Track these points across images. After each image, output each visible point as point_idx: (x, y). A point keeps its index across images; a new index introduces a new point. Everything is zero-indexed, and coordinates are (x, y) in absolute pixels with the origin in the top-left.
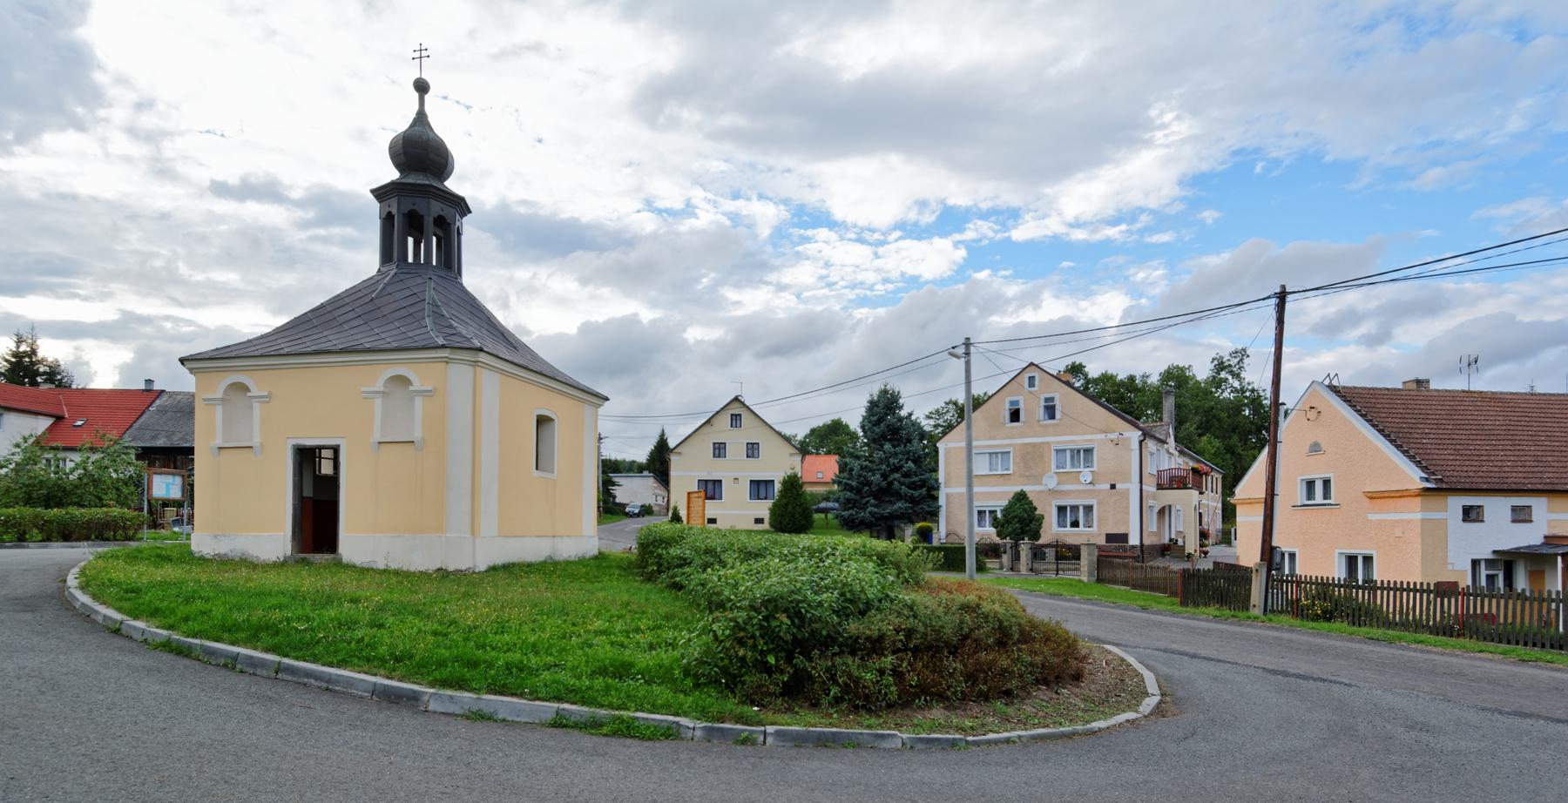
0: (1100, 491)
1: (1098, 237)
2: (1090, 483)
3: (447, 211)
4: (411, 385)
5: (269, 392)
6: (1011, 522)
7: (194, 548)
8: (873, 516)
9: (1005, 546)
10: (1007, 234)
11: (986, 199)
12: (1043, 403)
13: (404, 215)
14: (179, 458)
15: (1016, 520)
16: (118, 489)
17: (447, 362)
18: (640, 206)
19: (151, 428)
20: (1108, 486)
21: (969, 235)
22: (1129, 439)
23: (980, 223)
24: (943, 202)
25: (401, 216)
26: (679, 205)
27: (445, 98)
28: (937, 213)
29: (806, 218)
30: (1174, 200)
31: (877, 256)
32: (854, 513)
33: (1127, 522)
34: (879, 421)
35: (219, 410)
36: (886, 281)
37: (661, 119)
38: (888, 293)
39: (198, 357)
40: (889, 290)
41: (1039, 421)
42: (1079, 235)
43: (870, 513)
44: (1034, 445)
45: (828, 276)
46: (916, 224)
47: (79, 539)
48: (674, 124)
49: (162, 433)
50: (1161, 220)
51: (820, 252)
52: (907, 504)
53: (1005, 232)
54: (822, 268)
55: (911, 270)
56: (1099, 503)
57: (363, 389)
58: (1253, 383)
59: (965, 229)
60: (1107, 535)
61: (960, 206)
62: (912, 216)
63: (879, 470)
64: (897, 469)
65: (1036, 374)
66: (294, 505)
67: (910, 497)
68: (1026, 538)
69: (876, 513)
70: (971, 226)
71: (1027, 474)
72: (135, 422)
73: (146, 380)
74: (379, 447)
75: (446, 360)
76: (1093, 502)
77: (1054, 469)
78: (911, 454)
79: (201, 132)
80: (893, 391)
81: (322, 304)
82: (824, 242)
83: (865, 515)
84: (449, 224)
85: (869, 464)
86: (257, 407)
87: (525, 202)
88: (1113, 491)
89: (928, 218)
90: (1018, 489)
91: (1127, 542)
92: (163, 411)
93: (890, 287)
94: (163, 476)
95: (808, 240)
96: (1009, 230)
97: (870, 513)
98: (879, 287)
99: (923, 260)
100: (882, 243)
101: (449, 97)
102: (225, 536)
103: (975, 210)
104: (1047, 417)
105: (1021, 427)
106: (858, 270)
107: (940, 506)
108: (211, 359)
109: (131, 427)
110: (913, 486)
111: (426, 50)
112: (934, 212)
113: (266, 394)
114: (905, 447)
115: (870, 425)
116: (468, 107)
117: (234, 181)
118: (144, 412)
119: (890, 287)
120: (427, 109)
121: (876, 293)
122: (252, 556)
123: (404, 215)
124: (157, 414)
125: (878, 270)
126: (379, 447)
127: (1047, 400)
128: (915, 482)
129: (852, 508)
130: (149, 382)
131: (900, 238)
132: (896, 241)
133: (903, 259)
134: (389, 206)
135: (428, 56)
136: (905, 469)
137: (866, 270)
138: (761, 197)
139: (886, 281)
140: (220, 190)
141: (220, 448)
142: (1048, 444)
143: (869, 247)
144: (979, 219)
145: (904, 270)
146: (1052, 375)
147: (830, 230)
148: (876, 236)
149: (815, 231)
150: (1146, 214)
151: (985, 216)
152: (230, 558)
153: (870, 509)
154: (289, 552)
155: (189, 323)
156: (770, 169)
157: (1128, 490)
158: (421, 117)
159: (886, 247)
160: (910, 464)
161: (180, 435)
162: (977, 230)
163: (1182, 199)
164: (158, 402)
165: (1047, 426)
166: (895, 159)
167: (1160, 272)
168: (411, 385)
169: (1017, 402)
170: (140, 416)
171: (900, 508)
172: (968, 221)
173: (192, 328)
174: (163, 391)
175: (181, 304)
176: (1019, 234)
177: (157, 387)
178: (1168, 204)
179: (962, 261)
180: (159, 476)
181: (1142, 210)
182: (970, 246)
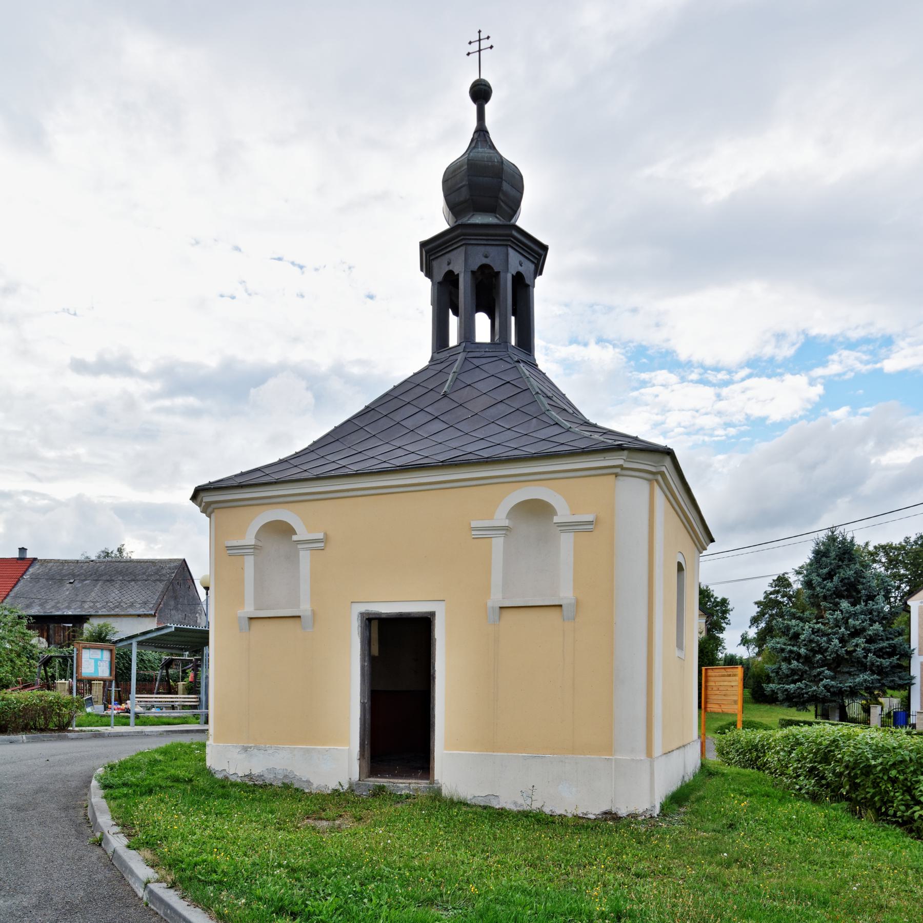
5: (326, 534)
7: (212, 761)
8: (828, 691)
10: (878, 366)
11: (857, 327)
13: (473, 272)
14: (51, 626)
16: (12, 661)
17: (617, 475)
19: (25, 596)
21: (834, 368)
23: (845, 353)
24: (804, 332)
25: (469, 274)
27: (280, 259)
28: (797, 346)
29: (644, 360)
31: (719, 397)
32: (802, 686)
34: (830, 576)
35: (249, 562)
36: (728, 425)
38: (729, 437)
40: (730, 435)
43: (825, 686)
45: (663, 423)
46: (772, 360)
47: (16, 731)
49: (36, 601)
51: (657, 396)
52: (875, 676)
53: (876, 363)
54: (657, 414)
55: (756, 411)
59: (827, 362)
61: (825, 336)
62: (769, 351)
63: (835, 634)
64: (856, 633)
67: (878, 666)
69: (832, 686)
70: (835, 357)
72: (11, 590)
73: (19, 549)
74: (500, 614)
75: (618, 470)
78: (875, 614)
79: (56, 313)
80: (845, 539)
81: (367, 407)
82: (662, 385)
83: (818, 689)
84: (528, 286)
85: (822, 627)
86: (305, 557)
87: (360, 362)
89: (787, 351)
92: (36, 579)
93: (732, 431)
94: (92, 651)
95: (644, 384)
97: (825, 686)
98: (720, 432)
99: (772, 399)
100: (726, 383)
103: (841, 339)
106: (697, 415)
107: (913, 678)
108: (241, 486)
109: (8, 595)
110: (880, 653)
112: (793, 344)
113: (320, 536)
114: (866, 605)
115: (820, 580)
116: (301, 267)
117: (90, 357)
118: (19, 580)
119: (732, 431)
121: (716, 439)
122: (300, 780)
123: (473, 272)
124: (30, 582)
125: (719, 413)
126: (500, 614)
128: (882, 648)
129: (800, 680)
130: (23, 550)
131: (749, 376)
132: (743, 380)
133: (749, 399)
134: (449, 264)
136: (870, 633)
137: (707, 414)
138: (600, 341)
139: (728, 425)
140: (80, 367)
141: (251, 619)
143: (712, 389)
144: (846, 348)
145: (749, 412)
147: (671, 372)
148: (722, 376)
149: (653, 374)
151: (852, 345)
152: (268, 782)
153: (825, 681)
154: (356, 776)
155: (43, 496)
156: (610, 309)
158: (481, 132)
159: (731, 387)
160: (877, 626)
161: (52, 603)
162: (841, 362)
164: (31, 570)
166: (757, 288)
170: (15, 585)
171: (865, 681)
172: (832, 351)
173: (46, 502)
174: (35, 559)
175: (40, 480)
176: (891, 365)
177: (29, 555)
179: (817, 399)
180: (88, 651)
182: (829, 383)
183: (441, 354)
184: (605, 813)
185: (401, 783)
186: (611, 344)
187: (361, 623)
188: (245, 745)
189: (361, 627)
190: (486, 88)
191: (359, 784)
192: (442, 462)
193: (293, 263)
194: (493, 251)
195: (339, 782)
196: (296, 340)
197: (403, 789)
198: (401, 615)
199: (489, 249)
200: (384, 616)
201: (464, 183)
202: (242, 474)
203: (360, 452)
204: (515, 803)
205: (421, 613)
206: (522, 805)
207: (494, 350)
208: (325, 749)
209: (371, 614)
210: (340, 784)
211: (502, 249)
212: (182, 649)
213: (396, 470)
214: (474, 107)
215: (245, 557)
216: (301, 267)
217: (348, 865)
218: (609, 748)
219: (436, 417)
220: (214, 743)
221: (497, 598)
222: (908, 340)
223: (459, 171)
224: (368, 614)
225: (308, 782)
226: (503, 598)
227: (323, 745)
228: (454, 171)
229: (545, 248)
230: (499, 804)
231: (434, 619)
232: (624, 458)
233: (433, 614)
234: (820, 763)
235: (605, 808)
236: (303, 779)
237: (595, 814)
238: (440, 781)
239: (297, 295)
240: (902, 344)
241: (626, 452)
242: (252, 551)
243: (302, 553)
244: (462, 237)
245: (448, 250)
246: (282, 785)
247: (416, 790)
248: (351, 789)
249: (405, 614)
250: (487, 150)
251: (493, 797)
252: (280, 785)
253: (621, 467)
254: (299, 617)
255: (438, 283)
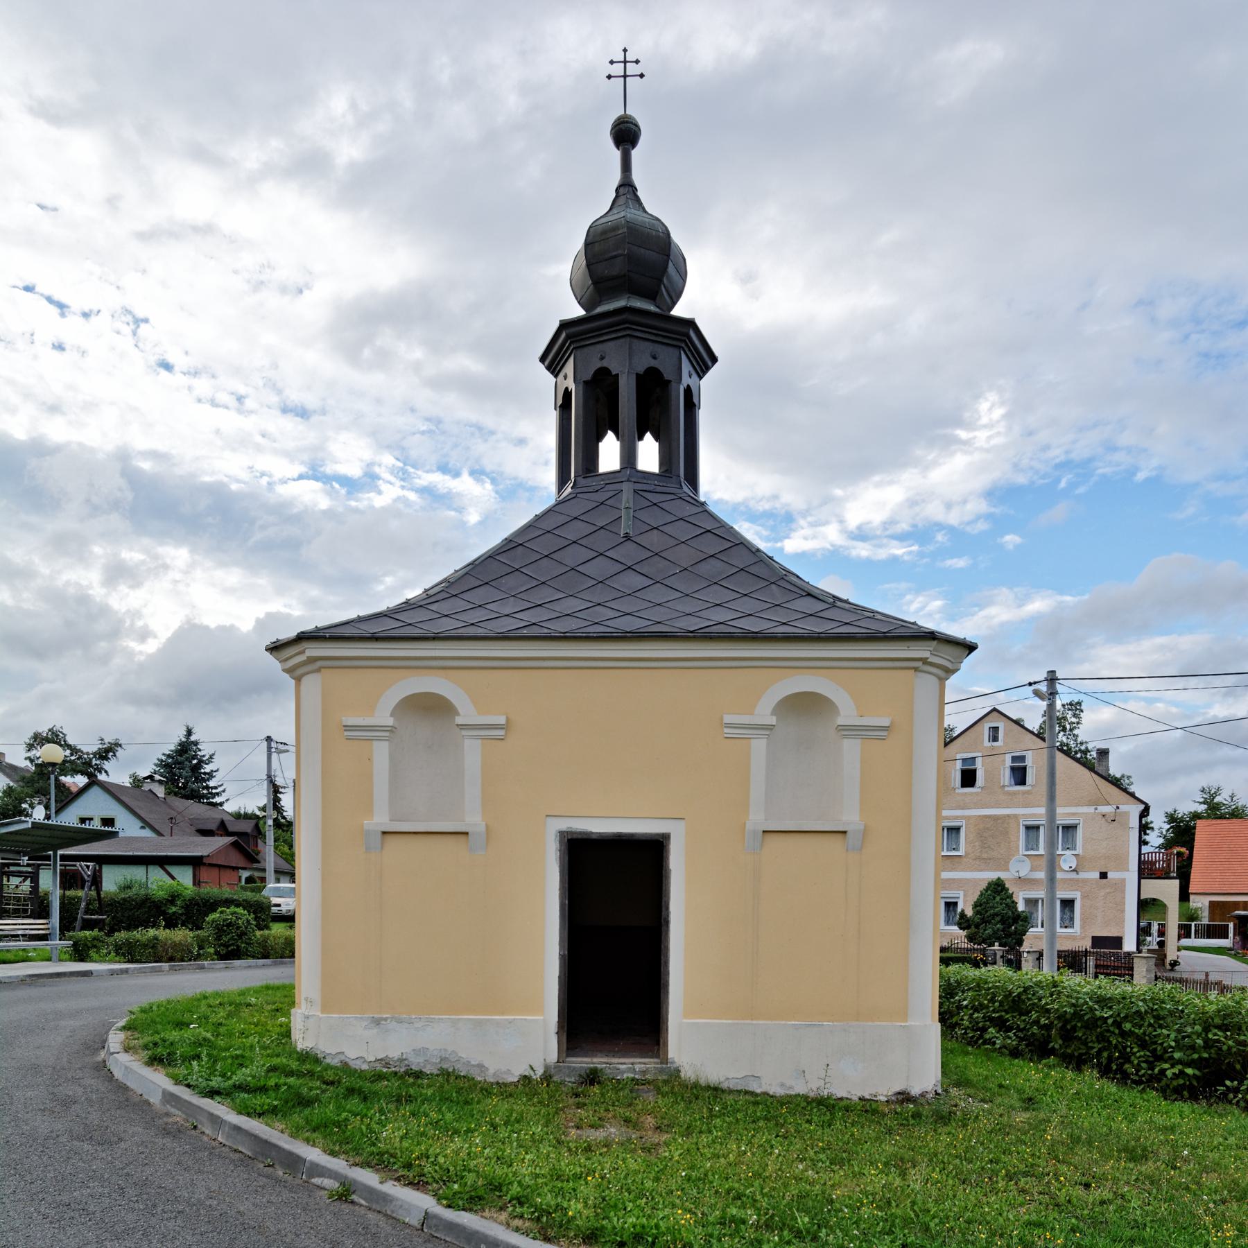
0: (1085, 881)
1: (882, 554)
2: (1073, 870)
3: (664, 360)
4: (458, 714)
5: (508, 720)
6: (990, 922)
9: (995, 954)
12: (1008, 763)
13: (586, 383)
15: (998, 919)
17: (916, 669)
18: (302, 469)
20: (1097, 875)
22: (1127, 814)
26: (355, 471)
27: (29, 289)
30: (978, 518)
33: (1121, 922)
37: (367, 353)
39: (347, 631)
41: (1004, 786)
42: (862, 551)
44: (995, 818)
48: (383, 360)
50: (959, 539)
56: (1084, 897)
57: (728, 719)
58: (1086, 742)
60: (1093, 937)
65: (1001, 724)
66: (562, 957)
68: (997, 944)
71: (985, 856)
75: (919, 664)
76: (1076, 895)
77: (1022, 850)
86: (472, 752)
87: (154, 455)
88: (1104, 881)
90: (993, 876)
91: (1121, 948)
96: (781, 540)
101: (37, 289)
102: (400, 1022)
103: (742, 508)
104: (1013, 783)
105: (977, 794)
111: (637, 62)
113: (502, 720)
120: (637, 177)
126: (763, 837)
127: (1014, 759)
134: (602, 358)
135: (642, 76)
142: (1016, 817)
144: (746, 520)
146: (1032, 732)
150: (943, 532)
154: (553, 1056)
157: (1124, 880)
158: (627, 189)
163: (988, 517)
165: (1014, 793)
167: (938, 603)
168: (458, 714)
169: (1023, 758)
178: (969, 523)
181: (940, 526)
183: (590, 479)
184: (899, 1093)
185: (622, 1064)
186: (488, 477)
187: (561, 845)
188: (376, 1016)
189: (560, 851)
190: (636, 129)
191: (560, 1066)
192: (692, 632)
193: (50, 300)
194: (663, 352)
195: (531, 1066)
196: (54, 409)
197: (623, 1072)
198: (619, 836)
199: (659, 349)
200: (594, 837)
201: (620, 252)
202: (361, 619)
203: (539, 605)
204: (782, 1085)
205: (651, 834)
206: (791, 1088)
207: (665, 484)
208: (507, 1020)
209: (575, 833)
210: (532, 1068)
211: (676, 351)
212: (18, 853)
213: (626, 637)
214: (616, 154)
215: (374, 742)
216: (61, 306)
217: (381, 1162)
218: (904, 1015)
219: (629, 567)
220: (322, 1013)
221: (757, 819)
222: (809, 519)
223: (613, 234)
224: (572, 833)
225: (481, 1066)
226: (766, 820)
227: (503, 1014)
228: (604, 232)
229: (714, 359)
230: (760, 1087)
231: (669, 843)
232: (931, 649)
233: (667, 837)
234: (1007, 1012)
235: (898, 1088)
236: (473, 1063)
237: (886, 1096)
238: (676, 1060)
239: (53, 345)
240: (802, 522)
241: (935, 643)
242: (387, 734)
243: (467, 742)
244: (627, 325)
245: (602, 339)
246: (438, 1072)
247: (644, 1072)
248: (547, 1077)
249: (626, 835)
250: (640, 213)
251: (753, 1078)
252: (436, 1072)
253: (924, 661)
254: (467, 833)
255: (584, 382)
